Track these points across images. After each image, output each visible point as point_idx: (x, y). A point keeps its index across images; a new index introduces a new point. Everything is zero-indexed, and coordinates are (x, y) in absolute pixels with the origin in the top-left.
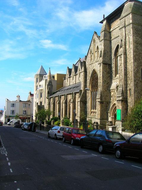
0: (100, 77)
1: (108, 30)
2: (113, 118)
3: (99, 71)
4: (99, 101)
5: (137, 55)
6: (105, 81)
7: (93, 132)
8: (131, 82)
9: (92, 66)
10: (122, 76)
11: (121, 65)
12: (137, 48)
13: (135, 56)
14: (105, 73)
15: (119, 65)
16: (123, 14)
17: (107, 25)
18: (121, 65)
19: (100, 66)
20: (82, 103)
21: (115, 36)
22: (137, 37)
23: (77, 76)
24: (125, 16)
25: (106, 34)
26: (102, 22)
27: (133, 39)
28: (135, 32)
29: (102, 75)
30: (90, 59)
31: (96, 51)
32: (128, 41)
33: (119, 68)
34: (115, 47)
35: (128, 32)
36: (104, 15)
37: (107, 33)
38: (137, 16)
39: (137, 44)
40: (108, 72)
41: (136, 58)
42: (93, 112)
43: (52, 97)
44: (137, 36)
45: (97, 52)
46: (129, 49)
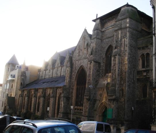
0: (41, 102)
1: (100, 29)
2: (100, 116)
3: (136, 87)
4: (87, 99)
5: (131, 57)
6: (94, 79)
7: (88, 94)
8: (124, 83)
9: (79, 62)
10: (116, 76)
11: (114, 65)
12: (131, 51)
13: (129, 58)
14: (95, 71)
15: (112, 65)
16: (119, 17)
17: (100, 25)
18: (114, 65)
19: (90, 64)
20: (65, 98)
21: (107, 36)
22: (132, 41)
23: (54, 70)
24: (122, 20)
25: (98, 33)
26: (94, 21)
27: (129, 42)
28: (131, 36)
29: (91, 73)
30: (78, 54)
31: (85, 48)
32: (123, 43)
33: (112, 68)
34: (107, 47)
35: (124, 35)
36: (97, 15)
37: (100, 32)
38: (133, 20)
39: (132, 47)
40: (98, 70)
41: (129, 60)
42: (77, 109)
43: (26, 90)
44: (132, 40)
45: (86, 49)
46: (124, 51)
